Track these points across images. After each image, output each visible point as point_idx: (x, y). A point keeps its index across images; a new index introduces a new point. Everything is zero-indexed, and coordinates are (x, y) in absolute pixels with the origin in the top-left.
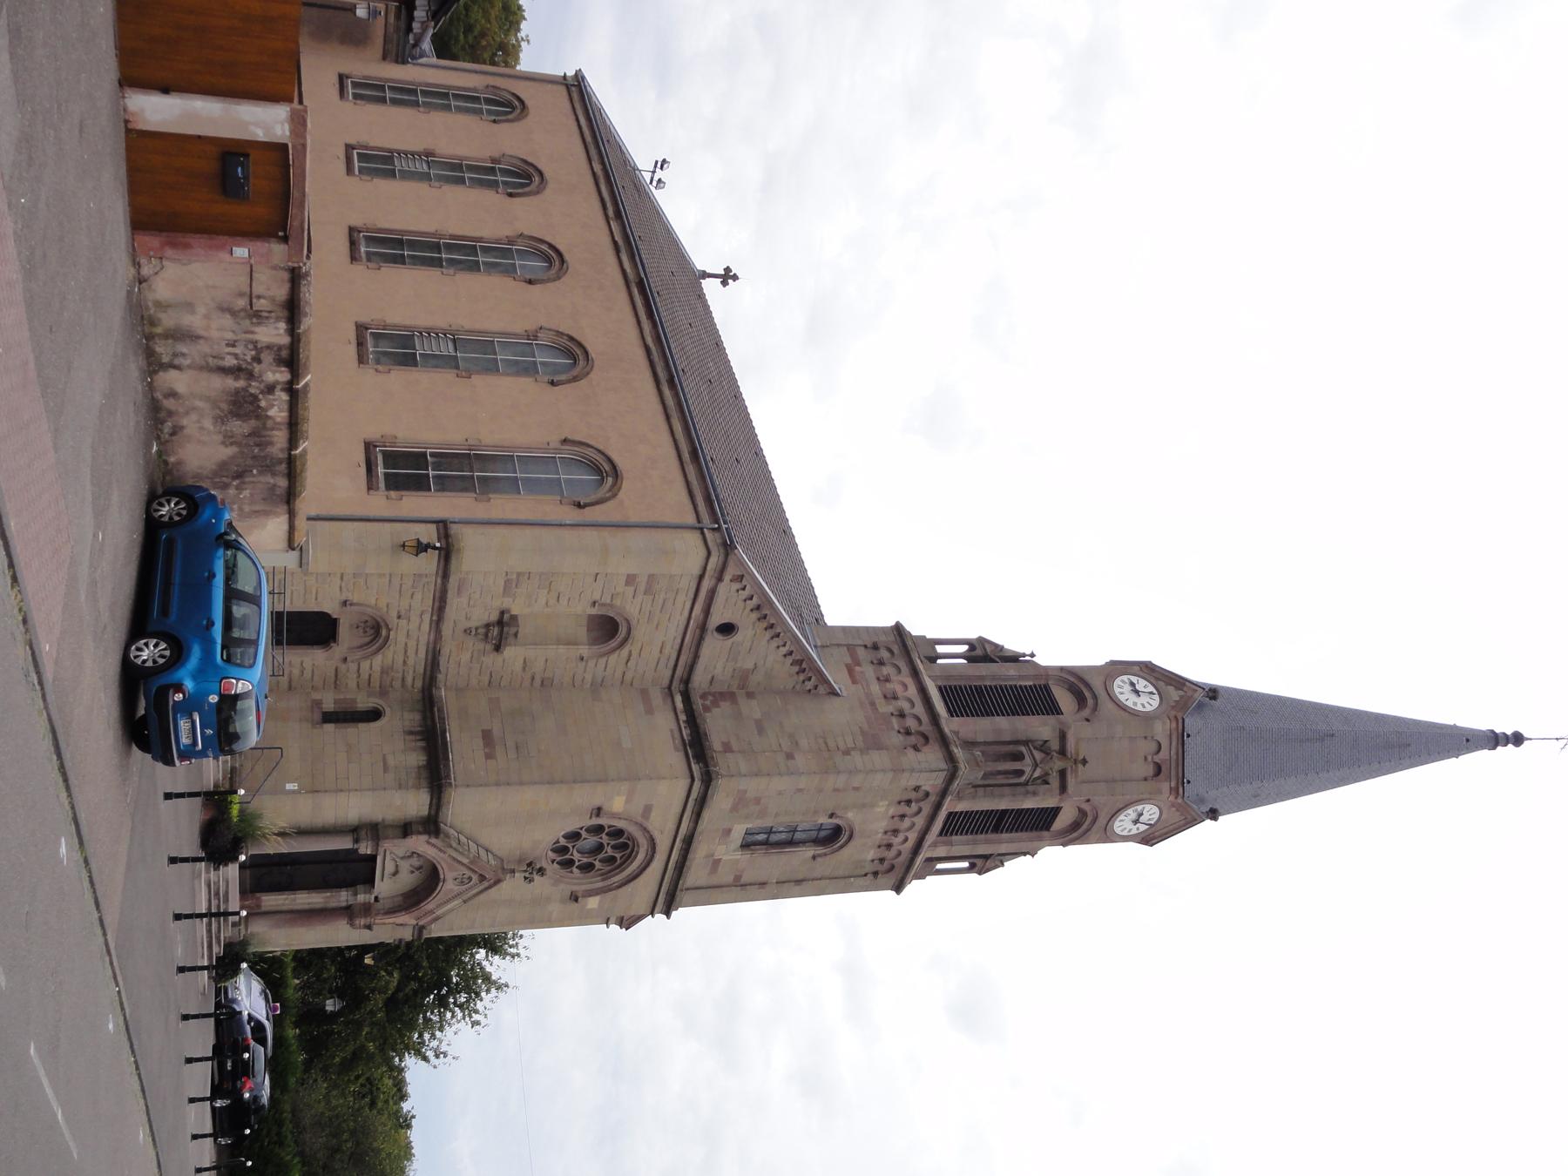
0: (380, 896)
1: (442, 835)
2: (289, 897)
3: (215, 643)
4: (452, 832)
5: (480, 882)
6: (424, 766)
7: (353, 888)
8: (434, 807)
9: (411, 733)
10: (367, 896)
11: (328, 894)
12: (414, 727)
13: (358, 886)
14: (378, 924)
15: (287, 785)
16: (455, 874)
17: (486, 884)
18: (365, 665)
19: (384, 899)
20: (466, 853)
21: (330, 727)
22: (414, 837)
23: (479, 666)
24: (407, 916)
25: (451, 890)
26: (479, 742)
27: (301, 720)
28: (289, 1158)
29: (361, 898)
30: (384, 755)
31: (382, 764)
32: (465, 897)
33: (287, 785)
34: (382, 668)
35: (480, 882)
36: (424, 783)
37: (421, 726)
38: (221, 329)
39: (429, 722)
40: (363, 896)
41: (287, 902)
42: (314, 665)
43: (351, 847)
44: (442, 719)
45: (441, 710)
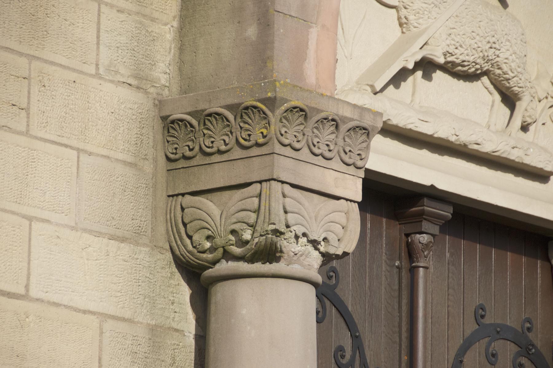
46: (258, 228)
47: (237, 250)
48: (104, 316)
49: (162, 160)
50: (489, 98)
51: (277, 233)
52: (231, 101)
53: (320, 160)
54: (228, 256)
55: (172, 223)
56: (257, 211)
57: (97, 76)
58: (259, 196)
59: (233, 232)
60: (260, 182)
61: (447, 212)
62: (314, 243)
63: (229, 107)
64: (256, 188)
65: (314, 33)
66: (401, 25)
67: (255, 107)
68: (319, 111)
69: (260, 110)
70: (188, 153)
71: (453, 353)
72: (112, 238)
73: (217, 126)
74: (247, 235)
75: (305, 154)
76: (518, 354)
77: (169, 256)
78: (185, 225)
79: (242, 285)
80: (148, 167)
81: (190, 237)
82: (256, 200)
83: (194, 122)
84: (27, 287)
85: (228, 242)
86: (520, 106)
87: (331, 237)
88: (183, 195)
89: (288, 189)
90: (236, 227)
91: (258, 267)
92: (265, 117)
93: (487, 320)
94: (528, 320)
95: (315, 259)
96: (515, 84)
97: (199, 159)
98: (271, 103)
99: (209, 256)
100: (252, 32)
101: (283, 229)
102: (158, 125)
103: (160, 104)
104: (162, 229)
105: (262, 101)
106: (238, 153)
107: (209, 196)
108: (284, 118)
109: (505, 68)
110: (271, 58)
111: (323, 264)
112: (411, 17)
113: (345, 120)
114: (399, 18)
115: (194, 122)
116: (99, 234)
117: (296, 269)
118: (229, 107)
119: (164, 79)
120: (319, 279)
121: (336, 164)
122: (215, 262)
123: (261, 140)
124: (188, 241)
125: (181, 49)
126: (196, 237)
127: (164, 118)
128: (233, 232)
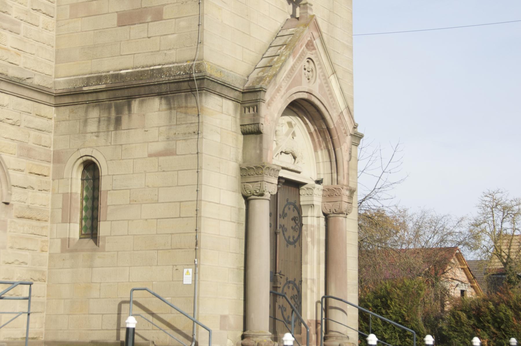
0: (316, 179)
1: (262, 84)
2: (309, 286)
3: (127, 73)
4: (254, 75)
5: (314, 49)
6: (169, 103)
7: (304, 210)
8: (226, 91)
9: (118, 121)
10: (315, 191)
11: (309, 239)
12: (109, 119)
13: (301, 203)
14: (348, 181)
15: (185, 282)
16: (304, 80)
17: (317, 42)
18: (16, 178)
19: (318, 174)
20: (283, 58)
21: (103, 228)
22: (262, 121)
23: (23, 24)
24: (343, 147)
25: (321, 87)
26: (136, 30)
27: (91, 267)
28: (448, 302)
29: (318, 200)
30: (150, 156)
31: (161, 158)
32: (330, 72)
33: (185, 282)
34: (20, 156)
35: (314, 49)
36: (192, 102)
37: (109, 107)
38: (467, 331)
39: (103, 96)
40: (315, 198)
41: (315, 289)
42: (11, 248)
43: (267, 203)
44: (99, 79)
45: (88, 81)
46: (260, 190)
47: (256, 194)
48: (232, 207)
49: (240, 175)
50: (291, 157)
51: (264, 191)
52: (255, 165)
53: (271, 177)
54: (253, 195)
55: (242, 188)
56: (260, 187)
57: (230, 160)
58: (261, 184)
59: (255, 191)
60: (261, 181)
61: (283, 181)
62: (270, 193)
63: (255, 167)
64: (260, 183)
65: (269, 152)
66: (277, 144)
67: (260, 167)
68: (271, 167)
69: (261, 168)
70: (245, 175)
71: (283, 208)
72: (233, 191)
73: (252, 170)
74: (258, 191)
75: (269, 176)
76: (294, 208)
77: (241, 194)
78: (245, 188)
79: (257, 201)
80: (238, 177)
81: (246, 191)
82: (260, 185)
83: (247, 169)
84: (220, 202)
85: (254, 192)
86: (297, 159)
87: (273, 191)
88: (244, 183)
89: (266, 183)
90: (256, 190)
91: (259, 197)
92: (262, 169)
93: (289, 201)
94: (295, 201)
95: (269, 195)
96: (296, 155)
97: (248, 176)
98: (263, 166)
99: (250, 195)
100: (258, 152)
101: (265, 190)
102: (239, 169)
103: (240, 165)
104: (240, 189)
105: (262, 166)
106: (256, 175)
107: (251, 183)
108: (266, 169)
109: (295, 152)
110: (262, 157)
111: (271, 196)
112: (279, 143)
113: (275, 169)
114: (276, 143)
115: (247, 169)
116: (230, 191)
117: (266, 198)
118: (255, 167)
119: (240, 160)
120: (270, 199)
121: (273, 177)
122: (250, 196)
123: (261, 173)
124: (245, 192)
125: (243, 154)
126: (247, 191)
127: (241, 168)
128: (255, 191)
